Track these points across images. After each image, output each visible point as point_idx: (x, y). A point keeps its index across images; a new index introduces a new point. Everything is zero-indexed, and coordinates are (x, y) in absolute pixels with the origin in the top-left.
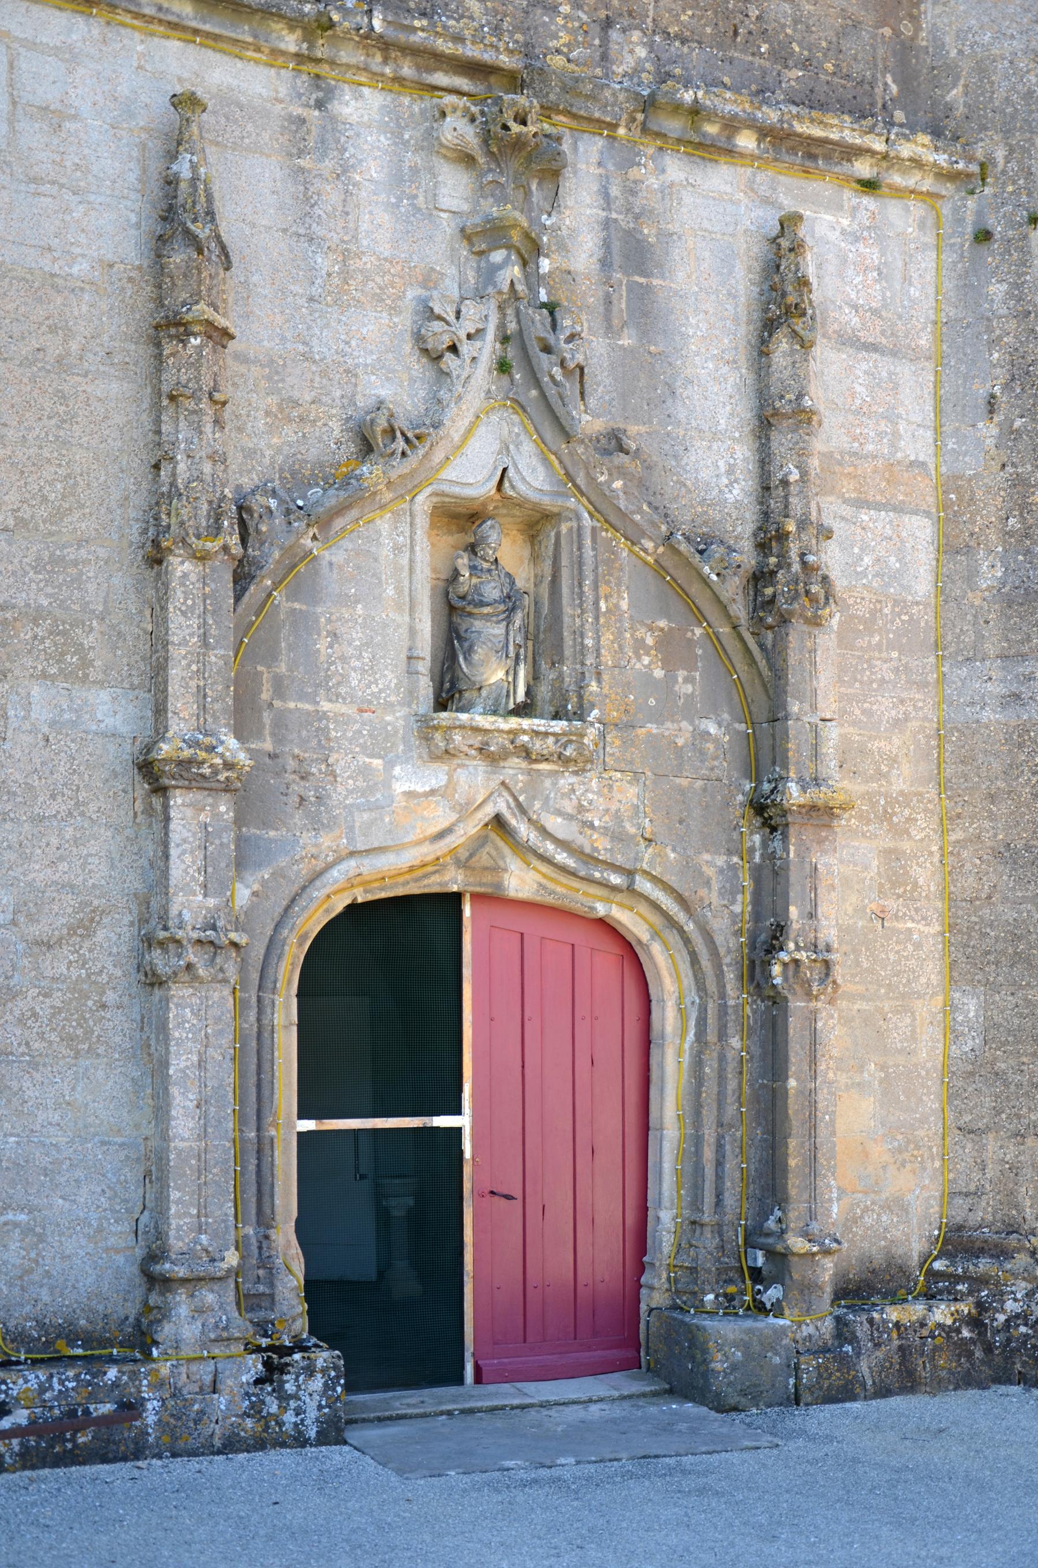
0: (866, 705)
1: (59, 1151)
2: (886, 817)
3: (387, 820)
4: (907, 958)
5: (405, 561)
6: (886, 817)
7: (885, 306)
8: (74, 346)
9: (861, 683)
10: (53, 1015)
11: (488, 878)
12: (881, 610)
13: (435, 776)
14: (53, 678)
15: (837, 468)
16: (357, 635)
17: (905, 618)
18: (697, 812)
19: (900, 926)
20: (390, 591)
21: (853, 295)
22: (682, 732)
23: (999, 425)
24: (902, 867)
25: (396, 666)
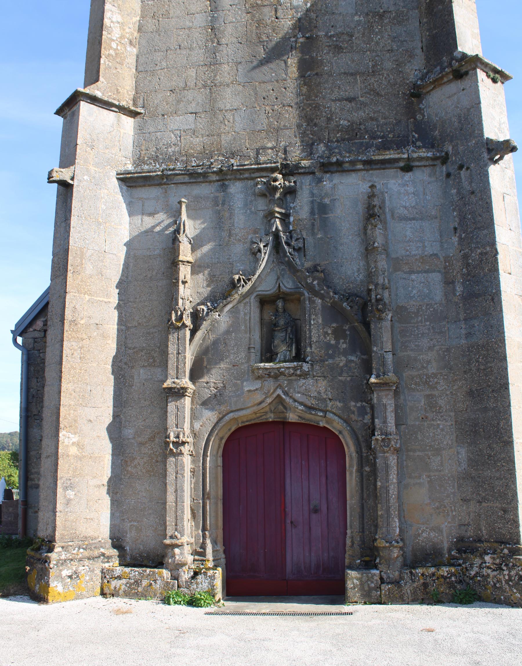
0: (417, 343)
1: (145, 505)
2: (427, 383)
4: (438, 435)
5: (248, 318)
6: (427, 383)
7: (417, 204)
8: (154, 273)
9: (414, 335)
10: (144, 464)
11: (282, 415)
12: (421, 308)
13: (258, 384)
14: (146, 366)
15: (401, 262)
16: (233, 343)
17: (431, 309)
19: (435, 423)
21: (404, 204)
22: (341, 361)
23: (458, 237)
24: (435, 401)
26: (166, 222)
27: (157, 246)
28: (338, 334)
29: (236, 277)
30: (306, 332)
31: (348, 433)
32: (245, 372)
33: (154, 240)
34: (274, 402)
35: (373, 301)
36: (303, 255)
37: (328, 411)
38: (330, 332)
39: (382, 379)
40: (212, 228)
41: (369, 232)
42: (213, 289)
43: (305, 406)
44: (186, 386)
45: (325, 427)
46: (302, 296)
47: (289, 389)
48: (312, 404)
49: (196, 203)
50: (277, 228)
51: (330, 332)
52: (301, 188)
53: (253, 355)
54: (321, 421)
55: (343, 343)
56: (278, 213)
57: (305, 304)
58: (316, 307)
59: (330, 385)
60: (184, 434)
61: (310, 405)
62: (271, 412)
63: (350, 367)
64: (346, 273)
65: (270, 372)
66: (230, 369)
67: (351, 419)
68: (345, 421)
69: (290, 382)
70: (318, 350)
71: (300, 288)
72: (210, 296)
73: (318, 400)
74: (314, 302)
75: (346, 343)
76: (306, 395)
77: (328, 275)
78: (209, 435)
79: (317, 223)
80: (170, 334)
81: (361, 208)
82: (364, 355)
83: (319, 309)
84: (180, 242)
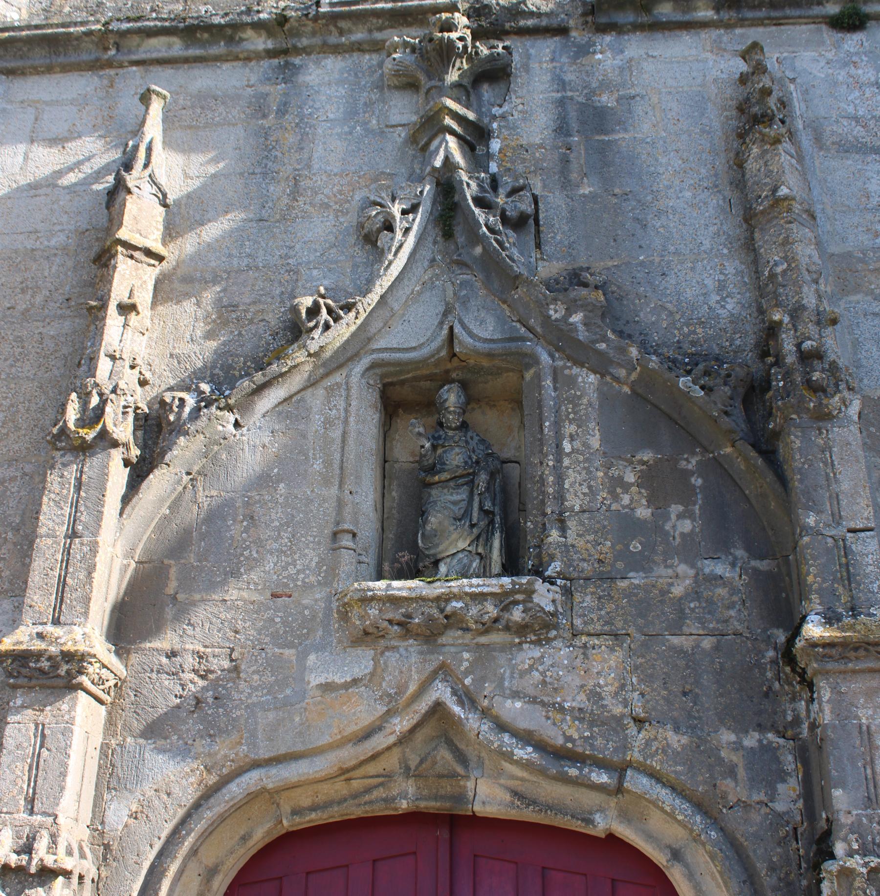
3: (297, 719)
5: (336, 434)
8: (39, 299)
11: (447, 788)
13: (360, 663)
15: (860, 266)
16: (277, 515)
18: (706, 679)
20: (318, 466)
21: (851, 109)
22: (679, 578)
25: (319, 543)
26: (99, 162)
27: (61, 224)
28: (660, 484)
29: (307, 301)
30: (542, 481)
31: (713, 857)
32: (314, 617)
33: (56, 206)
34: (419, 736)
35: (790, 359)
36: (532, 243)
37: (629, 765)
38: (630, 477)
39: (852, 627)
40: (241, 174)
41: (752, 165)
42: (224, 344)
43: (541, 746)
44: (82, 648)
45: (612, 839)
46: (528, 367)
47: (480, 681)
48: (569, 739)
49: (199, 111)
50: (447, 160)
51: (630, 477)
52: (527, 68)
53: (347, 557)
54: (601, 810)
55: (680, 516)
56: (455, 116)
57: (540, 387)
58: (580, 398)
59: (636, 668)
60: (54, 838)
61: (560, 741)
62: (407, 772)
63: (710, 602)
64: (679, 294)
65: (409, 616)
66: (259, 608)
67: (724, 796)
68: (699, 806)
69: (484, 654)
70: (591, 538)
71: (523, 339)
72: (213, 367)
73: (592, 724)
74: (571, 381)
75: (691, 516)
76: (543, 704)
77: (620, 299)
78: (161, 855)
79: (579, 158)
80: (52, 467)
81: (717, 120)
82: (762, 558)
83: (590, 404)
84: (129, 192)
